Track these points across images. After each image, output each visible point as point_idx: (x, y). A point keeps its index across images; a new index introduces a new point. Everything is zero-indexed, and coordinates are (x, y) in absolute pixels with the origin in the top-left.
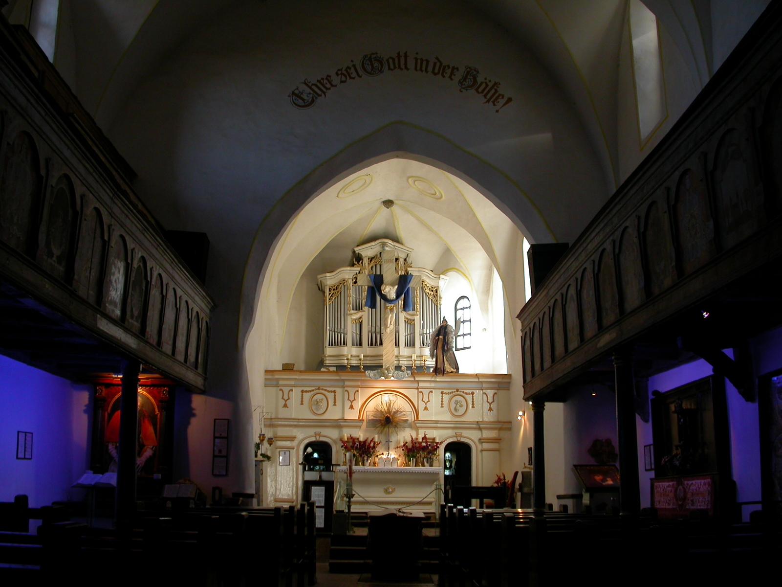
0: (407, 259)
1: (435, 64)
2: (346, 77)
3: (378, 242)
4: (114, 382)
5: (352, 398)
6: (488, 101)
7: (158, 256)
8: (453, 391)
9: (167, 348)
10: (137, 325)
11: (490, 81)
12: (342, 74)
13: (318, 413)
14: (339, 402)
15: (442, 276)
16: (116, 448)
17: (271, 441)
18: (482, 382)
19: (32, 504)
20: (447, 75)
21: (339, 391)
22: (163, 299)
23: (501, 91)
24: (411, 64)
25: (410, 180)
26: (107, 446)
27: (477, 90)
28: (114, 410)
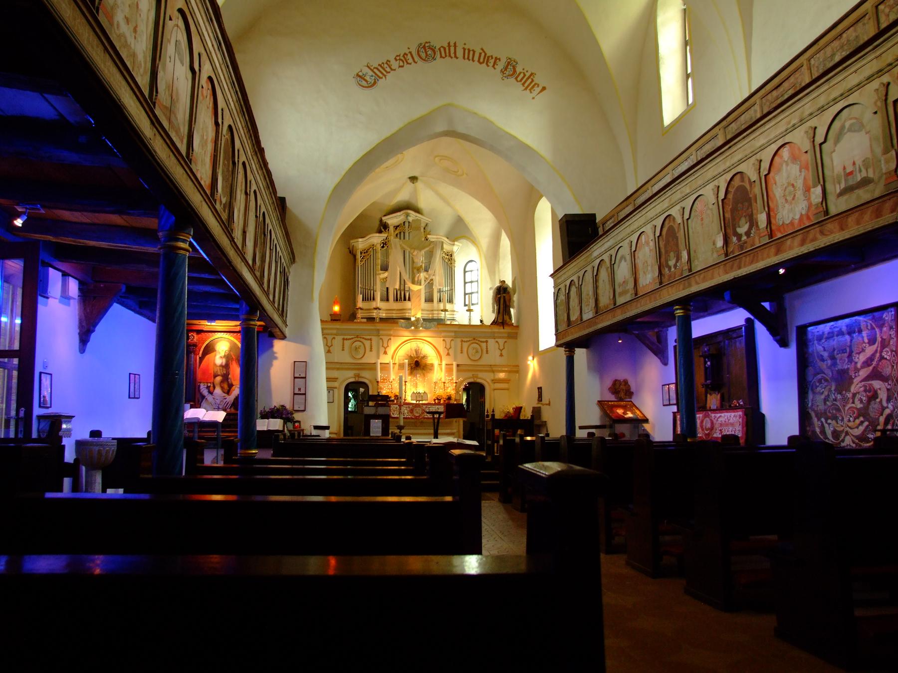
0: (426, 228)
2: (403, 62)
3: (402, 212)
5: (385, 345)
6: (526, 89)
11: (527, 71)
12: (400, 59)
13: (358, 357)
15: (456, 243)
18: (494, 332)
21: (374, 339)
23: (536, 80)
24: (460, 53)
25: (437, 159)
27: (516, 78)
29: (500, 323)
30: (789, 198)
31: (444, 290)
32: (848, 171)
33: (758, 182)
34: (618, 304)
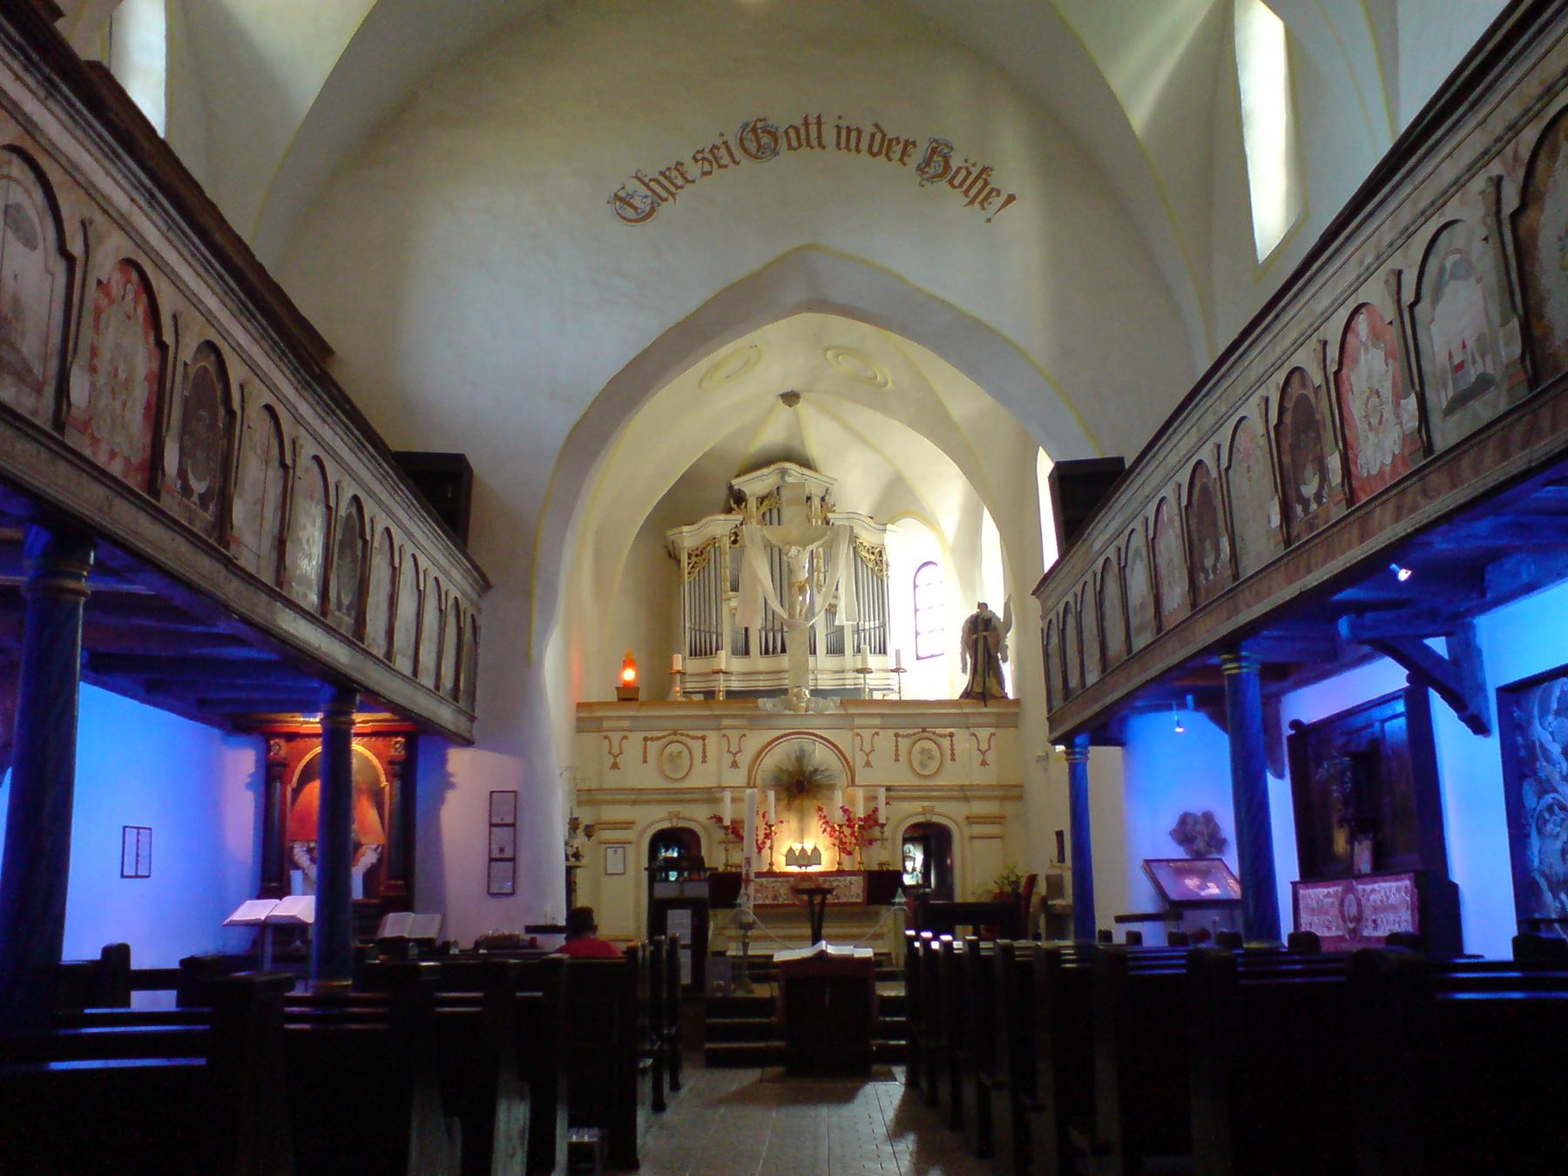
0: (826, 499)
1: (873, 136)
2: (711, 165)
3: (772, 467)
4: (301, 732)
6: (972, 202)
7: (384, 496)
8: (916, 730)
9: (403, 664)
10: (346, 622)
11: (974, 165)
12: (703, 159)
14: (711, 755)
15: (889, 526)
16: (310, 851)
17: (589, 831)
19: (139, 962)
20: (896, 156)
22: (395, 572)
24: (829, 136)
25: (829, 353)
26: (292, 848)
27: (951, 182)
28: (306, 778)
30: (1375, 421)
31: (867, 627)
32: (1457, 361)
33: (1324, 388)
34: (1135, 650)
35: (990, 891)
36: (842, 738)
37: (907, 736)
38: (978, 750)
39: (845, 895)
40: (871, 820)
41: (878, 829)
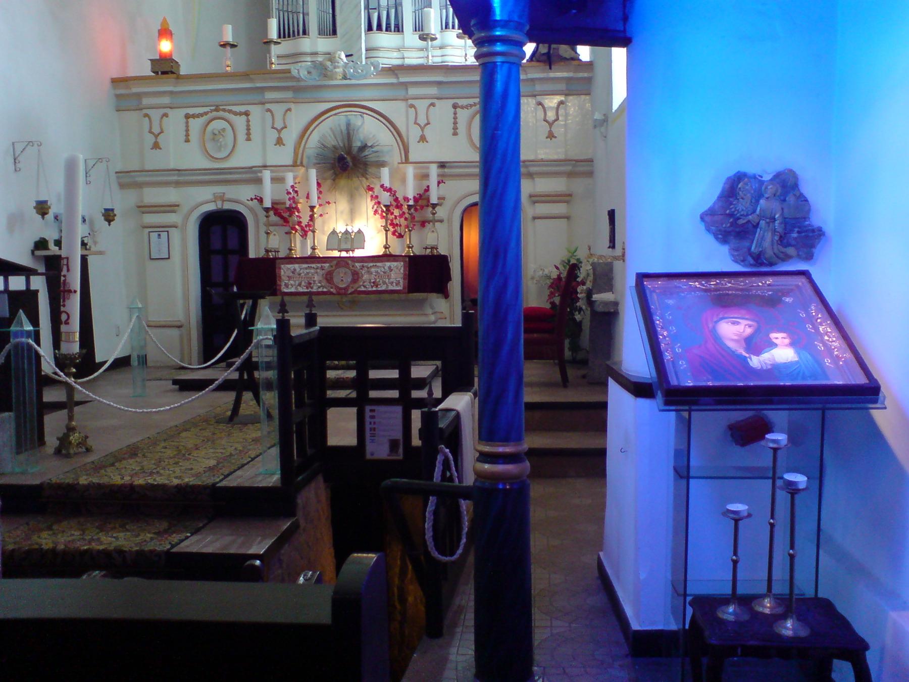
29: (544, 54)
35: (548, 277)
36: (395, 110)
37: (466, 107)
38: (545, 120)
39: (384, 283)
40: (422, 200)
41: (430, 209)
